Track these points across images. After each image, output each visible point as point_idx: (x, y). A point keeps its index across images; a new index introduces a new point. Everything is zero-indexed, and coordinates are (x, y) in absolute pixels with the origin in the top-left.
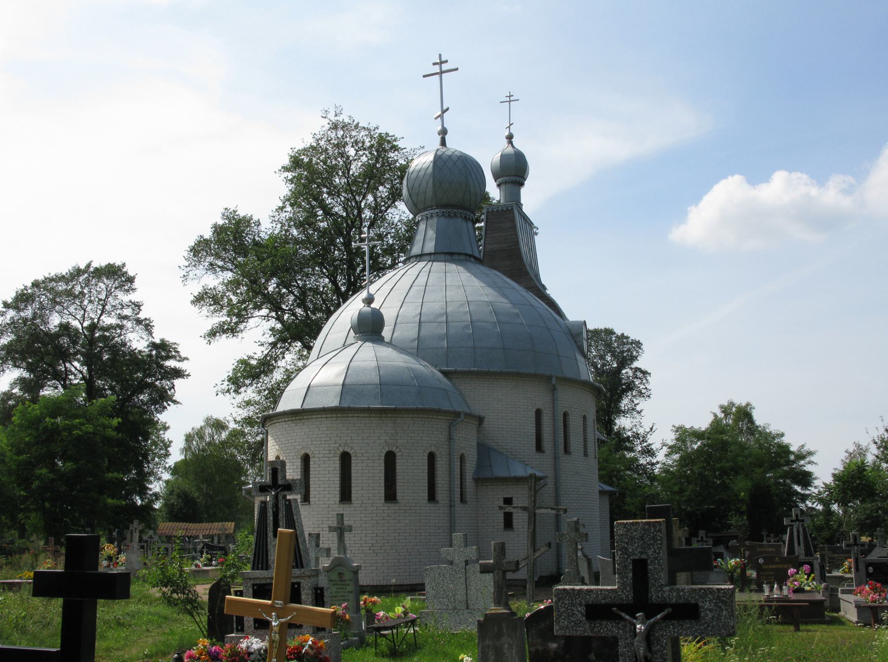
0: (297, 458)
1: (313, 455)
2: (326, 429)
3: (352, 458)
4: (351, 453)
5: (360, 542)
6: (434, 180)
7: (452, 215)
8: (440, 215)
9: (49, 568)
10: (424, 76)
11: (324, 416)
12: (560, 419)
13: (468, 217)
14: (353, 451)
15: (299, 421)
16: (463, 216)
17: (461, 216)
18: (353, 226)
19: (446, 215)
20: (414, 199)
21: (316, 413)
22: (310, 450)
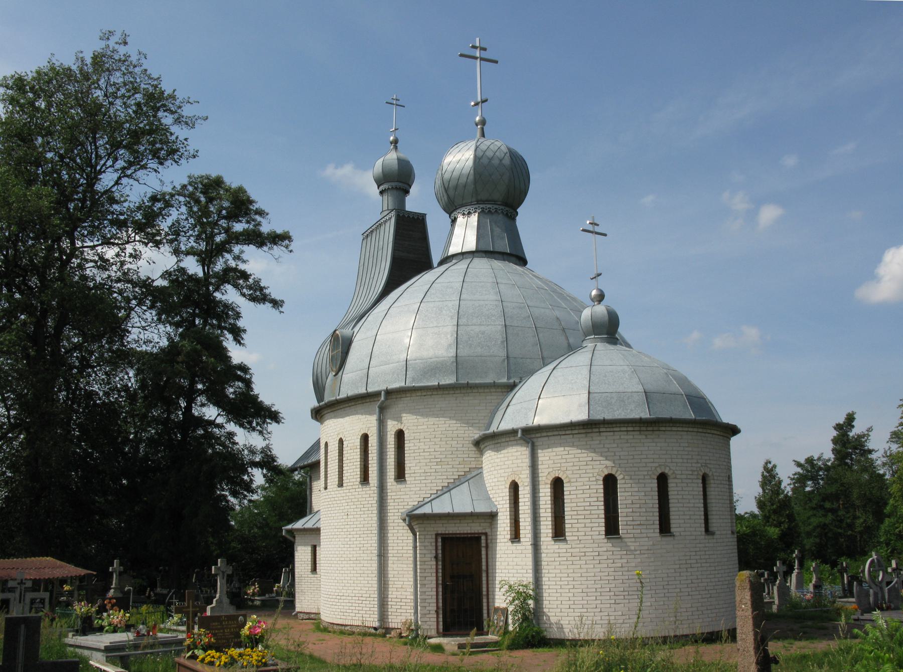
0: (651, 478)
1: (674, 476)
2: (687, 445)
3: (565, 485)
4: (602, 479)
5: (596, 594)
6: (475, 174)
7: (493, 211)
8: (493, 211)
9: (61, 567)
10: (496, 62)
11: (625, 429)
12: (391, 464)
13: (509, 215)
14: (565, 475)
15: (650, 433)
16: (505, 213)
17: (502, 212)
18: (17, 240)
19: (487, 211)
20: (451, 193)
21: (618, 425)
22: (670, 469)
